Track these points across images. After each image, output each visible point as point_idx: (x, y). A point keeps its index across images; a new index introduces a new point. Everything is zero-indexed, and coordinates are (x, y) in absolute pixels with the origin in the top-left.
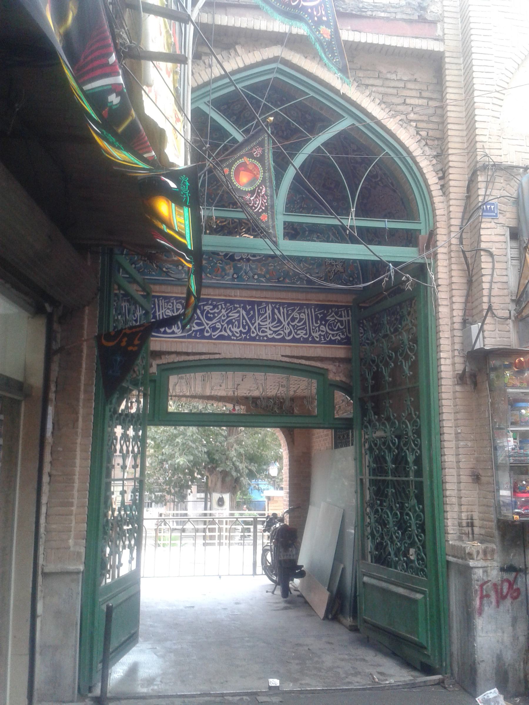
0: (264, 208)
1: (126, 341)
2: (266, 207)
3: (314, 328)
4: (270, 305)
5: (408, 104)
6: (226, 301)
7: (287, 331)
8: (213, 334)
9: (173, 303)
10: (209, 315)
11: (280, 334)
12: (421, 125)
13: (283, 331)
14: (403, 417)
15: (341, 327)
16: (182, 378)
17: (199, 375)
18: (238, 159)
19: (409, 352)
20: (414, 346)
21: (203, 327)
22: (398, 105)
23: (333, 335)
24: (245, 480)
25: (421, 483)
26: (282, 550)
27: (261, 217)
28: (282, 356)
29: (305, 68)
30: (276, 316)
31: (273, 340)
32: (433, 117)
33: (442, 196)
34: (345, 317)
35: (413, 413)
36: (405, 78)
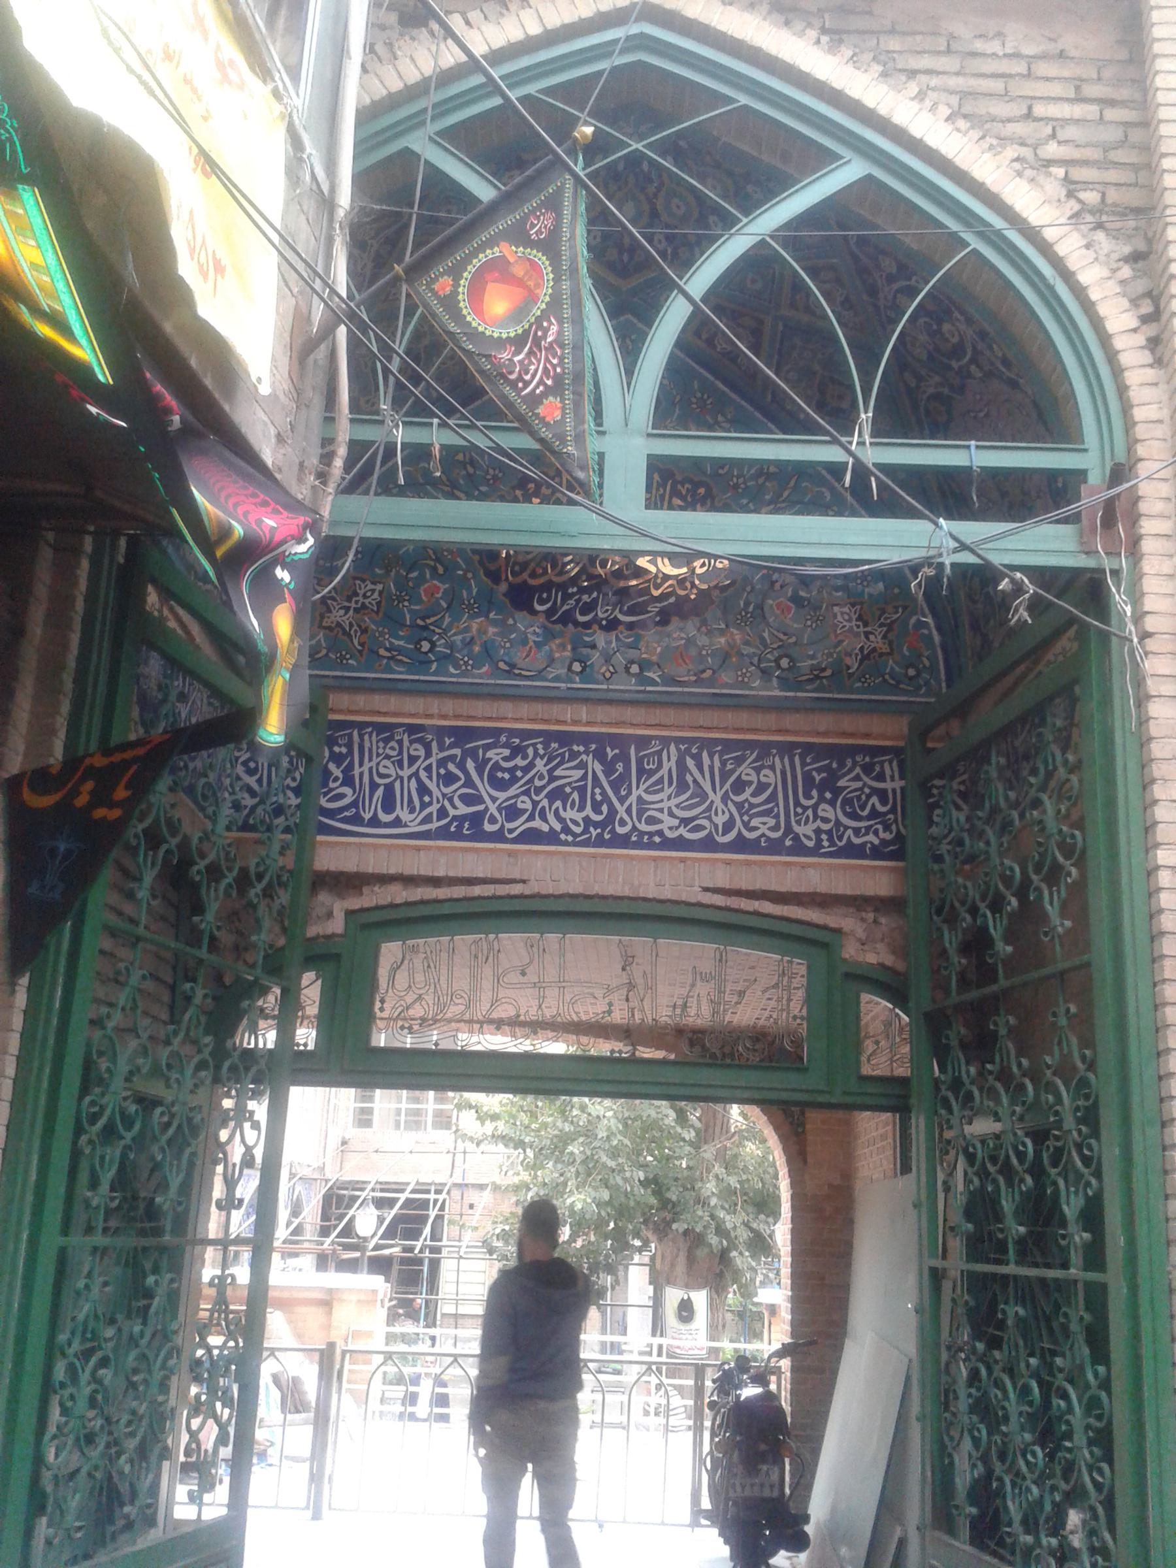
0: (549, 382)
1: (91, 793)
2: (558, 379)
3: (799, 810)
4: (672, 747)
5: (1041, 119)
6: (548, 737)
7: (720, 820)
8: (508, 826)
9: (400, 742)
10: (500, 775)
11: (700, 828)
12: (1079, 174)
13: (709, 818)
14: (1048, 1067)
15: (880, 808)
16: (414, 950)
17: (464, 941)
18: (482, 248)
19: (1061, 859)
20: (1073, 836)
21: (481, 807)
22: (1009, 120)
23: (857, 831)
24: (742, 1259)
25: (1103, 1288)
26: (739, 1469)
27: (540, 410)
28: (706, 889)
29: (722, 28)
30: (689, 778)
31: (680, 844)
32: (1119, 151)
33: (1151, 366)
34: (893, 779)
35: (1076, 1054)
36: (1029, 50)
